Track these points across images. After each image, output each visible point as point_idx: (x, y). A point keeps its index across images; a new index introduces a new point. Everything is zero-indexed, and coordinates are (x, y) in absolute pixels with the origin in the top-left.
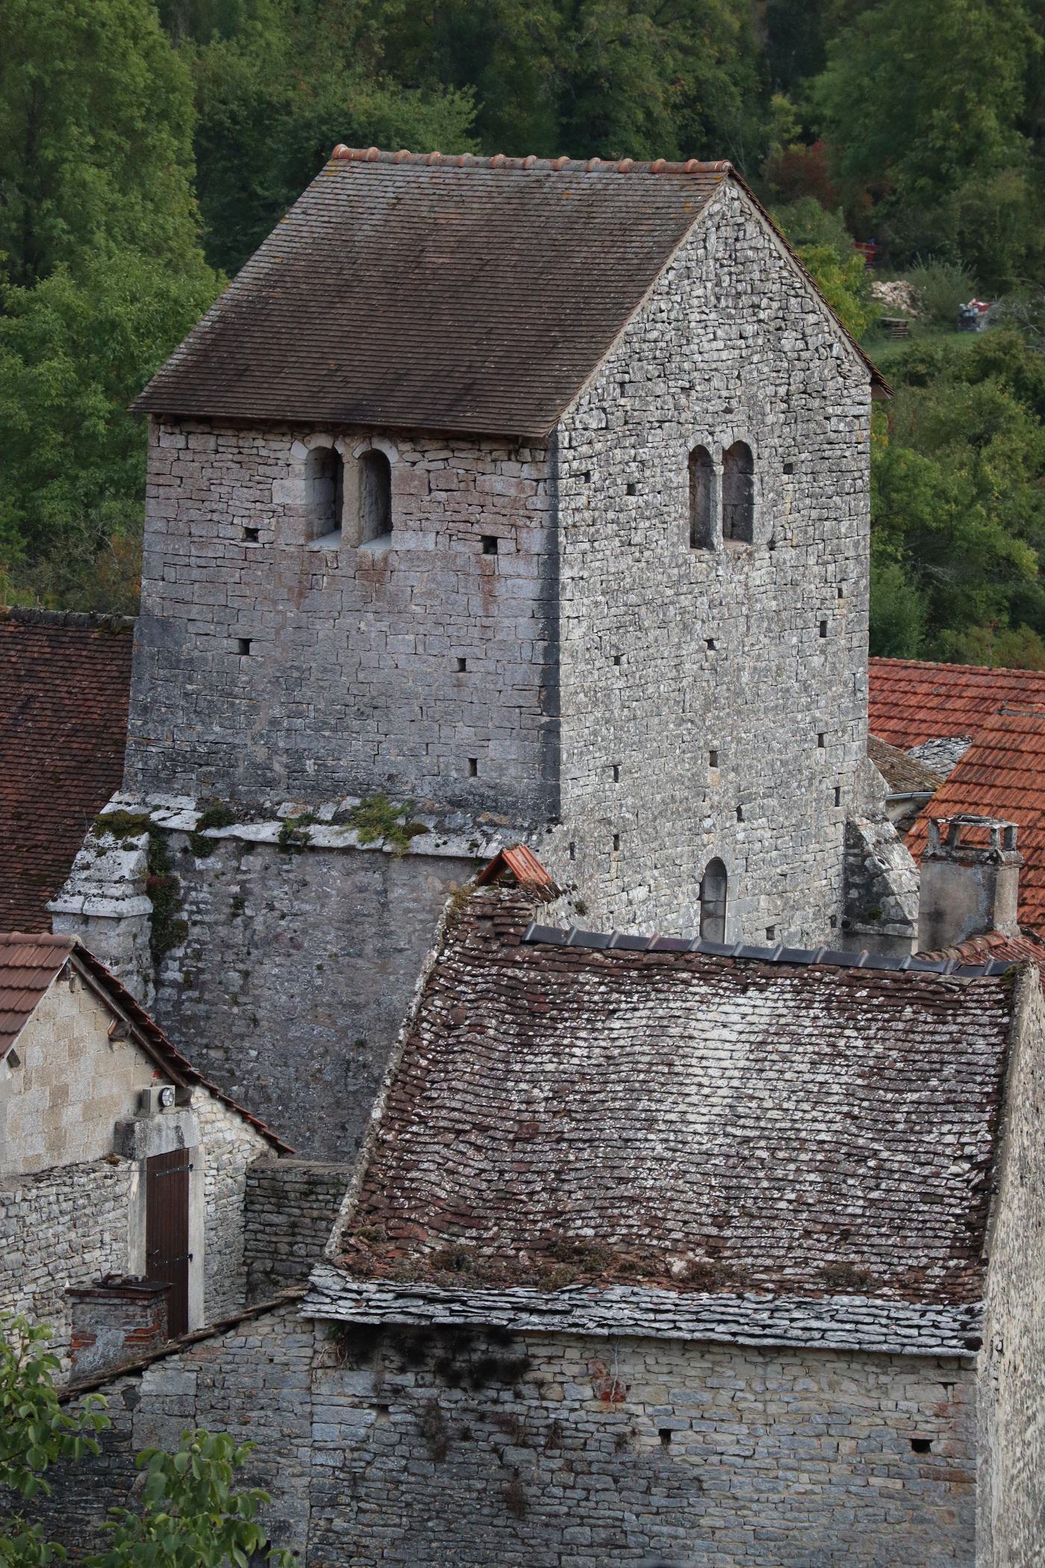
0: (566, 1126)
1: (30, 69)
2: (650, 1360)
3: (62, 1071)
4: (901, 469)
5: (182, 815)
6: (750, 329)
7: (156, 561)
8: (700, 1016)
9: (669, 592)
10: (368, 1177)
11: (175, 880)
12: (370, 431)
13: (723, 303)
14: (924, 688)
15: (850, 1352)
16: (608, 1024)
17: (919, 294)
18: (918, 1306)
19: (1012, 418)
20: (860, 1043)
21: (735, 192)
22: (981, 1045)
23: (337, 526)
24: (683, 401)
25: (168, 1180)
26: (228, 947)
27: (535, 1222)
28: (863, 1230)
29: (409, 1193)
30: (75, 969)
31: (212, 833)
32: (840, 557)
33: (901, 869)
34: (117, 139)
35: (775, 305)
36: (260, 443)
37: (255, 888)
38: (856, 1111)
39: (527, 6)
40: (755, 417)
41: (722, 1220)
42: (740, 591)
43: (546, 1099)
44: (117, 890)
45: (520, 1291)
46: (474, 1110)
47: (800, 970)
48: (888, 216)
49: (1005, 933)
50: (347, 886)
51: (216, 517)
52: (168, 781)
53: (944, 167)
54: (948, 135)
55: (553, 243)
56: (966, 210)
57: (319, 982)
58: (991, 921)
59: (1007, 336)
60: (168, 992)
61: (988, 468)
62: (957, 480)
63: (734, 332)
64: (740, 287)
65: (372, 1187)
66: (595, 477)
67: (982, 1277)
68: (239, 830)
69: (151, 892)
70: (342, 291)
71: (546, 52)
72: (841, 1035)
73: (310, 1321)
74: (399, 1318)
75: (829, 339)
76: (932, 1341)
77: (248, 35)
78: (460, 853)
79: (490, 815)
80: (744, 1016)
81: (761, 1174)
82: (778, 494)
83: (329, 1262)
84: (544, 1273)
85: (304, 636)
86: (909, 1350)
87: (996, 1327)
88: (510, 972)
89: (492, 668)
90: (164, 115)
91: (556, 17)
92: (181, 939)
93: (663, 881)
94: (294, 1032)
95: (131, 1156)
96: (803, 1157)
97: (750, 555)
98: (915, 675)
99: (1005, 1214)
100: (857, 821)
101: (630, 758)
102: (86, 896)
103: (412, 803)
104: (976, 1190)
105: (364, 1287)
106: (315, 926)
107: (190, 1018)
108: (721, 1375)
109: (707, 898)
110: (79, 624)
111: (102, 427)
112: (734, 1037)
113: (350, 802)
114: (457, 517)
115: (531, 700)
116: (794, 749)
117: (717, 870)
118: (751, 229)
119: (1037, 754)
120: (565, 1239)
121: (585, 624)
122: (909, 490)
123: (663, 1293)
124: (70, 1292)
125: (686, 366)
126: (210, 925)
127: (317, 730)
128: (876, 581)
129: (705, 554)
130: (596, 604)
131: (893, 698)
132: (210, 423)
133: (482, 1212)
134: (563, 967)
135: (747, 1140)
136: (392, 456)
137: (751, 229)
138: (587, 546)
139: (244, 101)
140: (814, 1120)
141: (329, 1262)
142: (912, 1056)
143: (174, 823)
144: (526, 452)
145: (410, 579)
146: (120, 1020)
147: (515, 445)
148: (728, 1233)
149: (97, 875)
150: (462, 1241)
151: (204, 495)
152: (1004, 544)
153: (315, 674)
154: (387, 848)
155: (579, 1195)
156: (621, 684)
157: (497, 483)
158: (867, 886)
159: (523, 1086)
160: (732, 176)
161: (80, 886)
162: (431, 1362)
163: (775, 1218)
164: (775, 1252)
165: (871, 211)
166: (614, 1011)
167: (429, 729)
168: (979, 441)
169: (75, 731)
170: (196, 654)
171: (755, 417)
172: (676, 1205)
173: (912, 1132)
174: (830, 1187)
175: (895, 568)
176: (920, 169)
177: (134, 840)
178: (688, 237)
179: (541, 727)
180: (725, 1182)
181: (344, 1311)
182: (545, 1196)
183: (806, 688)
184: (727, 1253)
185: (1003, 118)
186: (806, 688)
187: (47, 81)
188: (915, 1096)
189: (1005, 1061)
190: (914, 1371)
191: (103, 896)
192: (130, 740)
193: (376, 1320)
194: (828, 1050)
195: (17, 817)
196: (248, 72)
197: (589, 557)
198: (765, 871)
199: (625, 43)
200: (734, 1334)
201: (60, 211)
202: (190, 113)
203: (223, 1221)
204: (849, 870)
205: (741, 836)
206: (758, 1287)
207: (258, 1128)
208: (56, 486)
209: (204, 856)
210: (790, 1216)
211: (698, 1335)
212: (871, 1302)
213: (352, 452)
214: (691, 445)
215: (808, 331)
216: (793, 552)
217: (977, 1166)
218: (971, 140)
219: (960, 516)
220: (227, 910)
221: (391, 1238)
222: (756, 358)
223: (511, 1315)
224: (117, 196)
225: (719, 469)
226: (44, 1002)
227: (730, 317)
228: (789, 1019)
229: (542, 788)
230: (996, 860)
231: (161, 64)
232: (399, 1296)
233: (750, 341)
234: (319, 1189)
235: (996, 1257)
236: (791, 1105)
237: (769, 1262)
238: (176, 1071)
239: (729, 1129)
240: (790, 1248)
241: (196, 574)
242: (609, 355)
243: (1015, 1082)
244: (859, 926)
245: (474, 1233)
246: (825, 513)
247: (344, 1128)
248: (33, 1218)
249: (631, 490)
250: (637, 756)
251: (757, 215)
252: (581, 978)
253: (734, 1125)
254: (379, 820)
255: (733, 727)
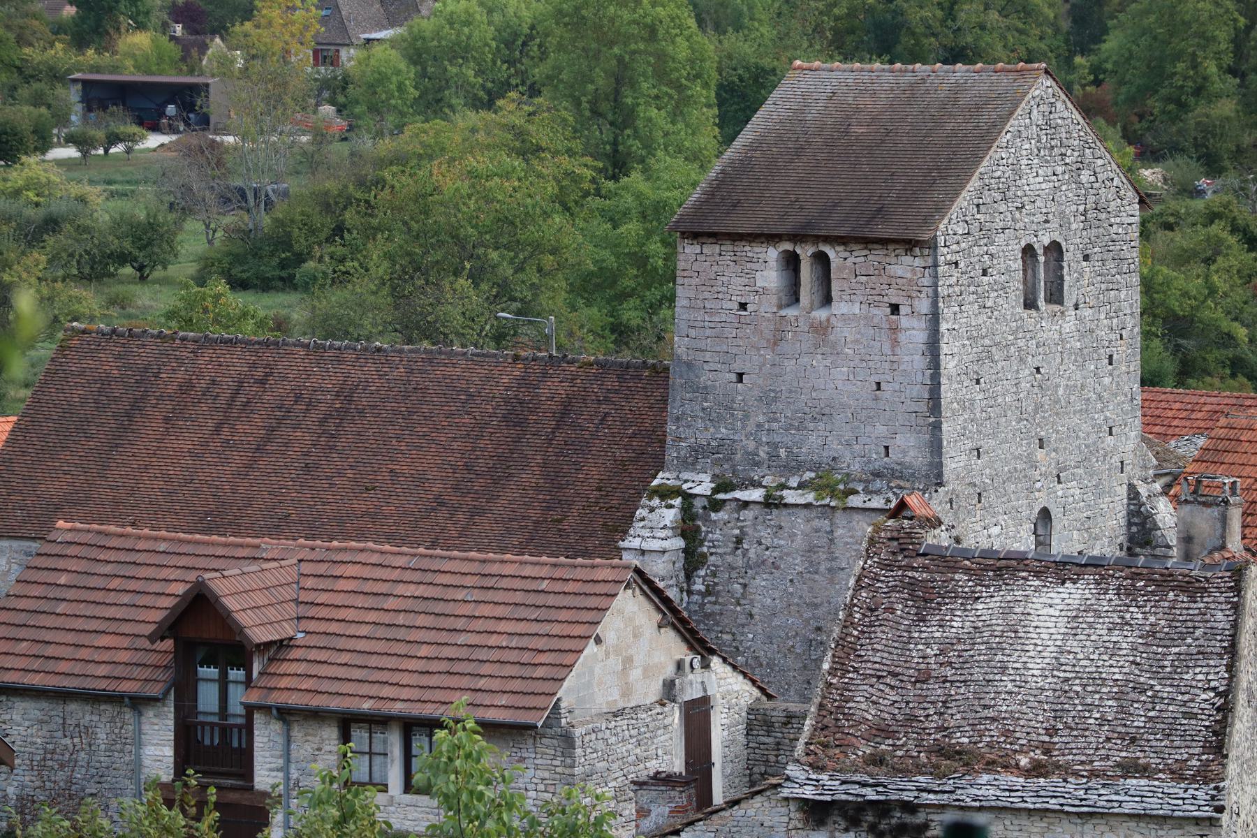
0: (949, 672)
1: (616, 50)
2: (1007, 822)
3: (629, 647)
4: (1160, 279)
5: (702, 485)
6: (1059, 170)
7: (683, 325)
8: (1034, 600)
9: (1011, 338)
10: (821, 706)
11: (699, 527)
12: (818, 239)
13: (1042, 153)
14: (1177, 406)
15: (1139, 816)
16: (974, 606)
17: (1168, 176)
18: (1182, 785)
19: (1229, 247)
20: (1140, 616)
21: (1049, 82)
22: (1220, 616)
23: (798, 300)
24: (1018, 215)
25: (697, 716)
26: (733, 568)
27: (930, 734)
28: (1145, 736)
29: (848, 717)
30: (635, 582)
31: (721, 496)
32: (1121, 314)
33: (1165, 513)
34: (669, 91)
35: (1076, 154)
36: (747, 248)
37: (750, 531)
38: (1138, 659)
39: (921, 8)
40: (1064, 225)
41: (1052, 731)
42: (1057, 336)
43: (936, 655)
44: (662, 534)
45: (921, 779)
46: (888, 662)
47: (1099, 569)
48: (1148, 129)
49: (1233, 550)
50: (807, 528)
51: (720, 296)
52: (693, 464)
53: (1183, 98)
54: (1186, 78)
55: (933, 117)
56: (1198, 124)
57: (791, 590)
58: (1224, 542)
59: (1225, 198)
60: (695, 598)
61: (1215, 278)
62: (1195, 285)
63: (1050, 172)
64: (1053, 143)
65: (824, 713)
66: (962, 265)
67: (1224, 766)
68: (738, 494)
69: (683, 535)
70: (799, 152)
71: (933, 34)
72: (1127, 611)
73: (787, 799)
74: (844, 797)
75: (1111, 175)
76: (1192, 808)
77: (750, 30)
78: (879, 506)
79: (898, 482)
80: (1063, 600)
81: (1077, 702)
82: (1080, 274)
83: (798, 761)
84: (937, 767)
85: (777, 370)
86: (1176, 814)
87: (1234, 798)
88: (910, 574)
89: (897, 388)
90: (698, 76)
91: (939, 14)
92: (703, 564)
93: (1010, 522)
94: (776, 622)
95: (674, 701)
96: (1104, 690)
97: (1062, 313)
98: (1171, 397)
99: (1238, 726)
100: (1135, 482)
101: (987, 444)
102: (643, 537)
103: (848, 475)
104: (1218, 710)
105: (820, 777)
106: (788, 554)
107: (710, 614)
108: (1054, 831)
109: (1039, 533)
110: (636, 368)
111: (660, 262)
112: (1057, 613)
113: (809, 475)
114: (873, 292)
115: (923, 407)
116: (1093, 437)
117: (1045, 514)
118: (1059, 105)
119: (1251, 442)
120: (950, 745)
121: (956, 358)
122: (1164, 292)
123: (1015, 779)
124: (633, 782)
125: (1019, 193)
126: (721, 555)
127: (787, 430)
128: (1145, 349)
129: (1033, 312)
130: (964, 346)
131: (1157, 412)
132: (716, 237)
133: (895, 729)
134: (944, 570)
135: (1067, 680)
136: (831, 254)
137: (1059, 105)
138: (957, 309)
139: (747, 68)
140: (1111, 666)
141: (798, 761)
142: (1174, 624)
143: (697, 490)
144: (917, 250)
145: (844, 332)
146: (665, 614)
147: (909, 245)
148: (1056, 740)
149: (650, 525)
150: (883, 747)
151: (713, 282)
152: (1226, 324)
153: (785, 394)
154: (833, 504)
155: (958, 716)
156: (981, 397)
157: (897, 270)
158: (1143, 524)
159: (920, 647)
160: (1047, 72)
161: (639, 531)
162: (865, 825)
163: (1087, 729)
164: (1087, 752)
165: (1137, 126)
166: (978, 598)
167: (859, 427)
168: (1208, 261)
169: (634, 435)
170: (709, 383)
171: (1064, 225)
172: (1022, 723)
173: (1176, 672)
174: (1122, 709)
175: (1157, 342)
176: (1168, 100)
177: (672, 502)
178: (1019, 111)
179: (930, 425)
180: (1054, 707)
181: (808, 793)
182: (936, 717)
183: (1100, 398)
184: (1056, 753)
185: (1220, 67)
186: (1100, 398)
187: (627, 58)
188: (1177, 650)
189: (1235, 626)
190: (1181, 827)
191: (654, 537)
192: (669, 439)
193: (828, 798)
194: (1119, 621)
195: (599, 489)
196: (748, 51)
197: (958, 316)
198: (1077, 515)
199: (982, 27)
200: (1062, 805)
201: (636, 135)
202: (715, 75)
203: (733, 741)
204: (1130, 514)
205: (1060, 493)
206: (1076, 774)
207: (754, 682)
208: (634, 302)
209: (716, 511)
210: (1097, 728)
211: (1038, 806)
212: (1151, 783)
213: (805, 252)
214: (1023, 244)
215: (1098, 170)
216: (1091, 311)
217: (1219, 694)
218: (1199, 80)
219: (1197, 308)
220: (732, 545)
221: (837, 746)
222: (1064, 188)
223: (916, 794)
224: (670, 126)
225: (1042, 259)
226: (616, 603)
227: (1047, 162)
228: (1093, 601)
229: (931, 464)
230: (1226, 502)
231: (691, 44)
232: (843, 783)
233: (1060, 177)
234: (794, 721)
235: (1233, 753)
236: (1095, 657)
237: (1084, 758)
238: (701, 646)
239: (1055, 673)
240: (1097, 749)
241: (708, 332)
242: (969, 187)
243: (1243, 640)
244: (1138, 550)
245: (890, 741)
246: (1111, 286)
247: (809, 683)
248: (613, 740)
249: (985, 273)
250: (992, 443)
251: (1063, 97)
252: (956, 577)
253: (1059, 670)
254: (828, 486)
255: (1054, 423)
